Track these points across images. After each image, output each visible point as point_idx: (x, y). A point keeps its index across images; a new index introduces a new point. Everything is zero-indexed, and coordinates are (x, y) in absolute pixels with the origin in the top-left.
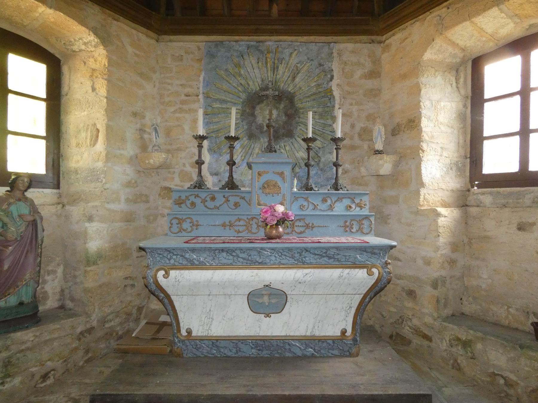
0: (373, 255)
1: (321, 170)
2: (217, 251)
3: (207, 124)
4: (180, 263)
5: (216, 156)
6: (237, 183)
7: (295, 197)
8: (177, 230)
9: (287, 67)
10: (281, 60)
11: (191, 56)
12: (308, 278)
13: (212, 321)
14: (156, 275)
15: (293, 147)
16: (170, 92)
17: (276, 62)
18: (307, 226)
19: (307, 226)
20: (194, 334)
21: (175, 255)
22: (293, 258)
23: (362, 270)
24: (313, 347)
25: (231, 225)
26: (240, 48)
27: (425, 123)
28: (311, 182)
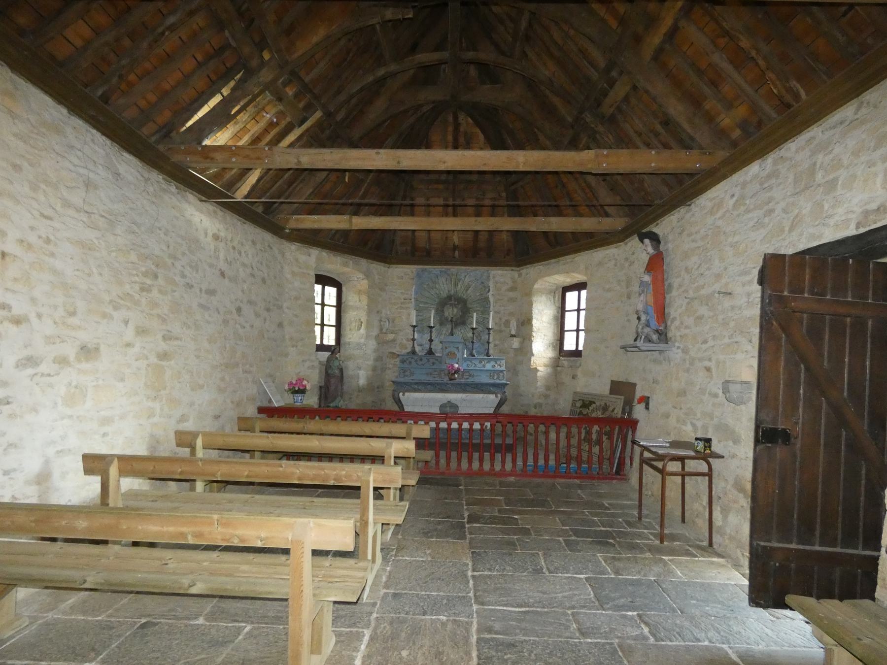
7: (465, 360)
27: (534, 322)
28: (474, 352)
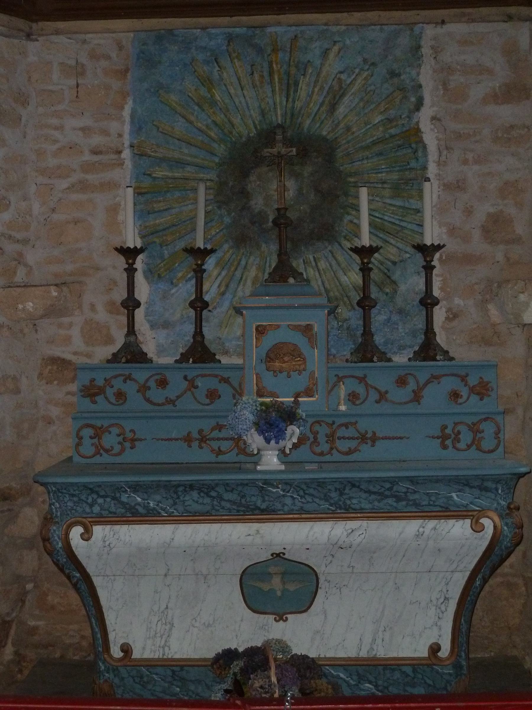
0: (484, 493)
1: (401, 312)
2: (181, 489)
3: (142, 213)
4: (111, 513)
5: (162, 286)
6: (213, 348)
8: (93, 450)
9: (316, 82)
10: (303, 67)
11: (104, 63)
12: (356, 539)
13: (171, 629)
14: (67, 534)
15: (334, 263)
16: (57, 146)
17: (293, 71)
18: (363, 438)
19: (363, 438)
20: (136, 654)
21: (102, 497)
22: (326, 500)
23: (461, 522)
24: (374, 680)
25: (203, 439)
26: (212, 43)
